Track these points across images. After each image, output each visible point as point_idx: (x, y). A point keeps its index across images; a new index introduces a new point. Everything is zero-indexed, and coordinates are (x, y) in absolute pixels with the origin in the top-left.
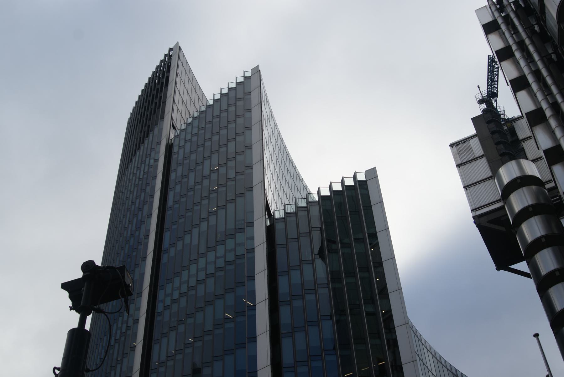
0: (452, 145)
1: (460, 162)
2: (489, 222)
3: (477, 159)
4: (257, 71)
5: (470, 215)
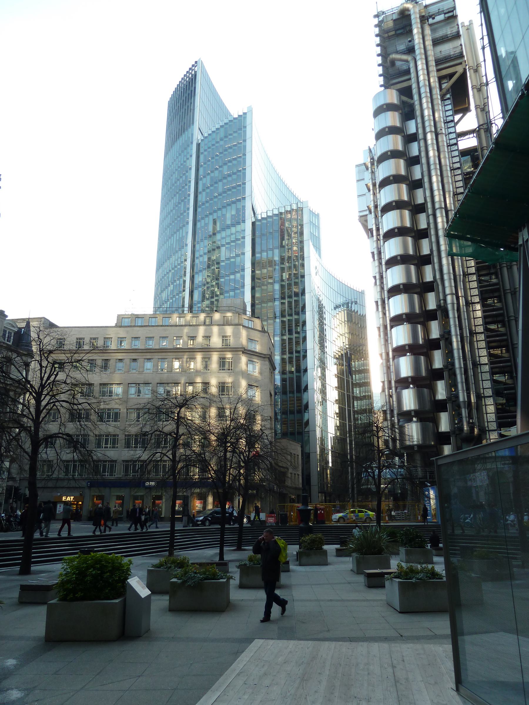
4: (250, 110)
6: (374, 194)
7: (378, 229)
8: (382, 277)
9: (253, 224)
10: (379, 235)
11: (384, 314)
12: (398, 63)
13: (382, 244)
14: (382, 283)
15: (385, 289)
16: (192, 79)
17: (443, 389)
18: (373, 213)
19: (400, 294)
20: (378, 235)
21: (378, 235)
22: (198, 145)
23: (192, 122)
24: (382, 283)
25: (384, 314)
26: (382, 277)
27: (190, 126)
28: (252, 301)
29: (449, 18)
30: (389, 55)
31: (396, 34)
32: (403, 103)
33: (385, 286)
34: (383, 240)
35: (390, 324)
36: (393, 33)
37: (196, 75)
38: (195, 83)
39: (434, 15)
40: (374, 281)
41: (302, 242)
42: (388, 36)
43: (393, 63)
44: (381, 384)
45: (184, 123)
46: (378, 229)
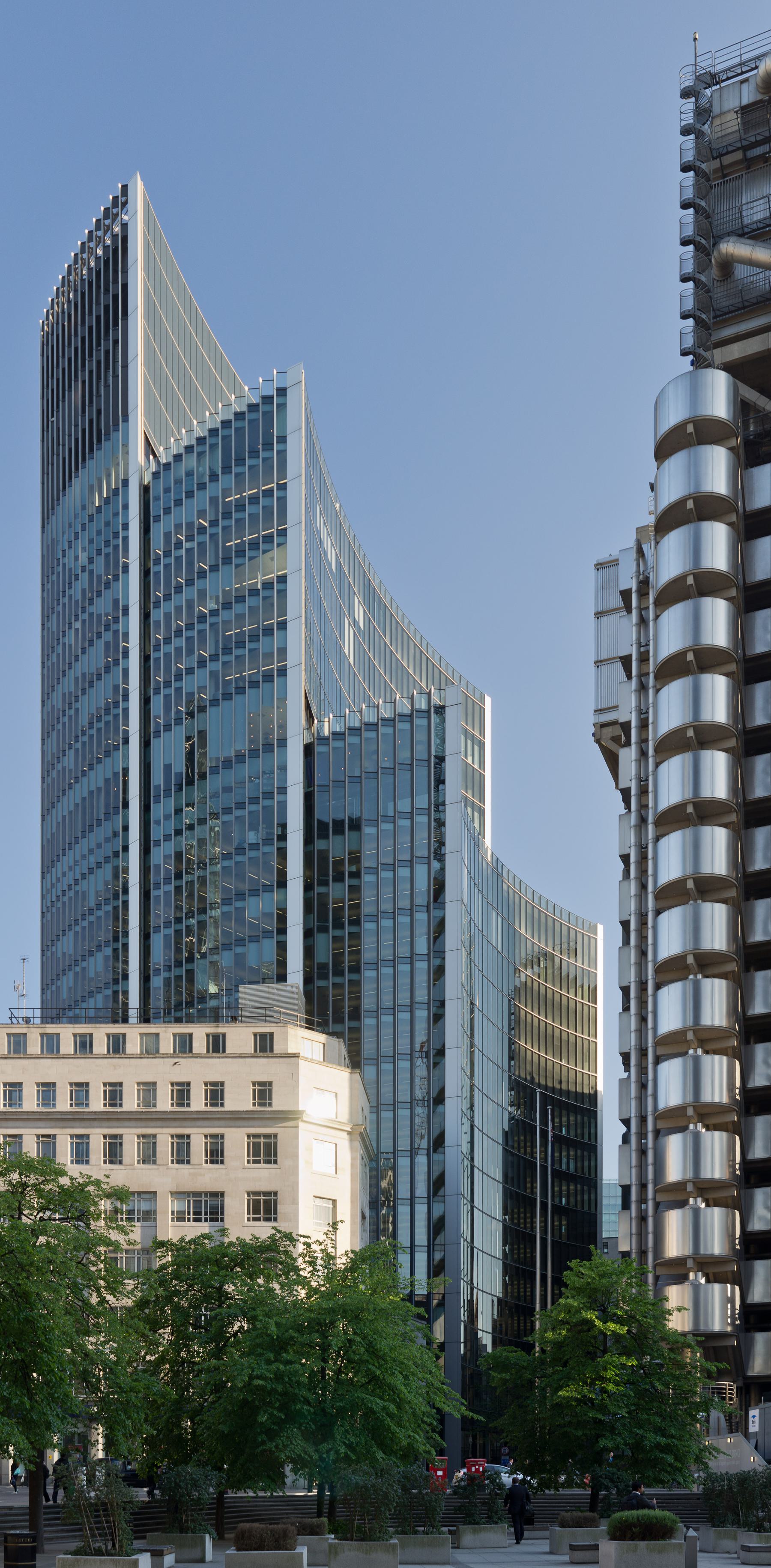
1: (600, 609)
6: (643, 621)
7: (644, 725)
8: (643, 857)
9: (308, 750)
10: (646, 741)
11: (643, 953)
12: (742, 272)
13: (651, 767)
14: (643, 871)
15: (650, 888)
16: (115, 251)
17: (766, 1208)
18: (634, 612)
19: (688, 827)
20: (643, 741)
21: (643, 741)
22: (145, 490)
24: (643, 871)
25: (643, 953)
26: (643, 857)
28: (305, 966)
30: (717, 240)
31: (745, 159)
33: (650, 880)
34: (655, 756)
35: (655, 979)
36: (739, 155)
38: (125, 271)
40: (622, 866)
41: (440, 806)
42: (722, 167)
43: (727, 266)
44: (597, 745)
45: (99, 412)
46: (644, 725)
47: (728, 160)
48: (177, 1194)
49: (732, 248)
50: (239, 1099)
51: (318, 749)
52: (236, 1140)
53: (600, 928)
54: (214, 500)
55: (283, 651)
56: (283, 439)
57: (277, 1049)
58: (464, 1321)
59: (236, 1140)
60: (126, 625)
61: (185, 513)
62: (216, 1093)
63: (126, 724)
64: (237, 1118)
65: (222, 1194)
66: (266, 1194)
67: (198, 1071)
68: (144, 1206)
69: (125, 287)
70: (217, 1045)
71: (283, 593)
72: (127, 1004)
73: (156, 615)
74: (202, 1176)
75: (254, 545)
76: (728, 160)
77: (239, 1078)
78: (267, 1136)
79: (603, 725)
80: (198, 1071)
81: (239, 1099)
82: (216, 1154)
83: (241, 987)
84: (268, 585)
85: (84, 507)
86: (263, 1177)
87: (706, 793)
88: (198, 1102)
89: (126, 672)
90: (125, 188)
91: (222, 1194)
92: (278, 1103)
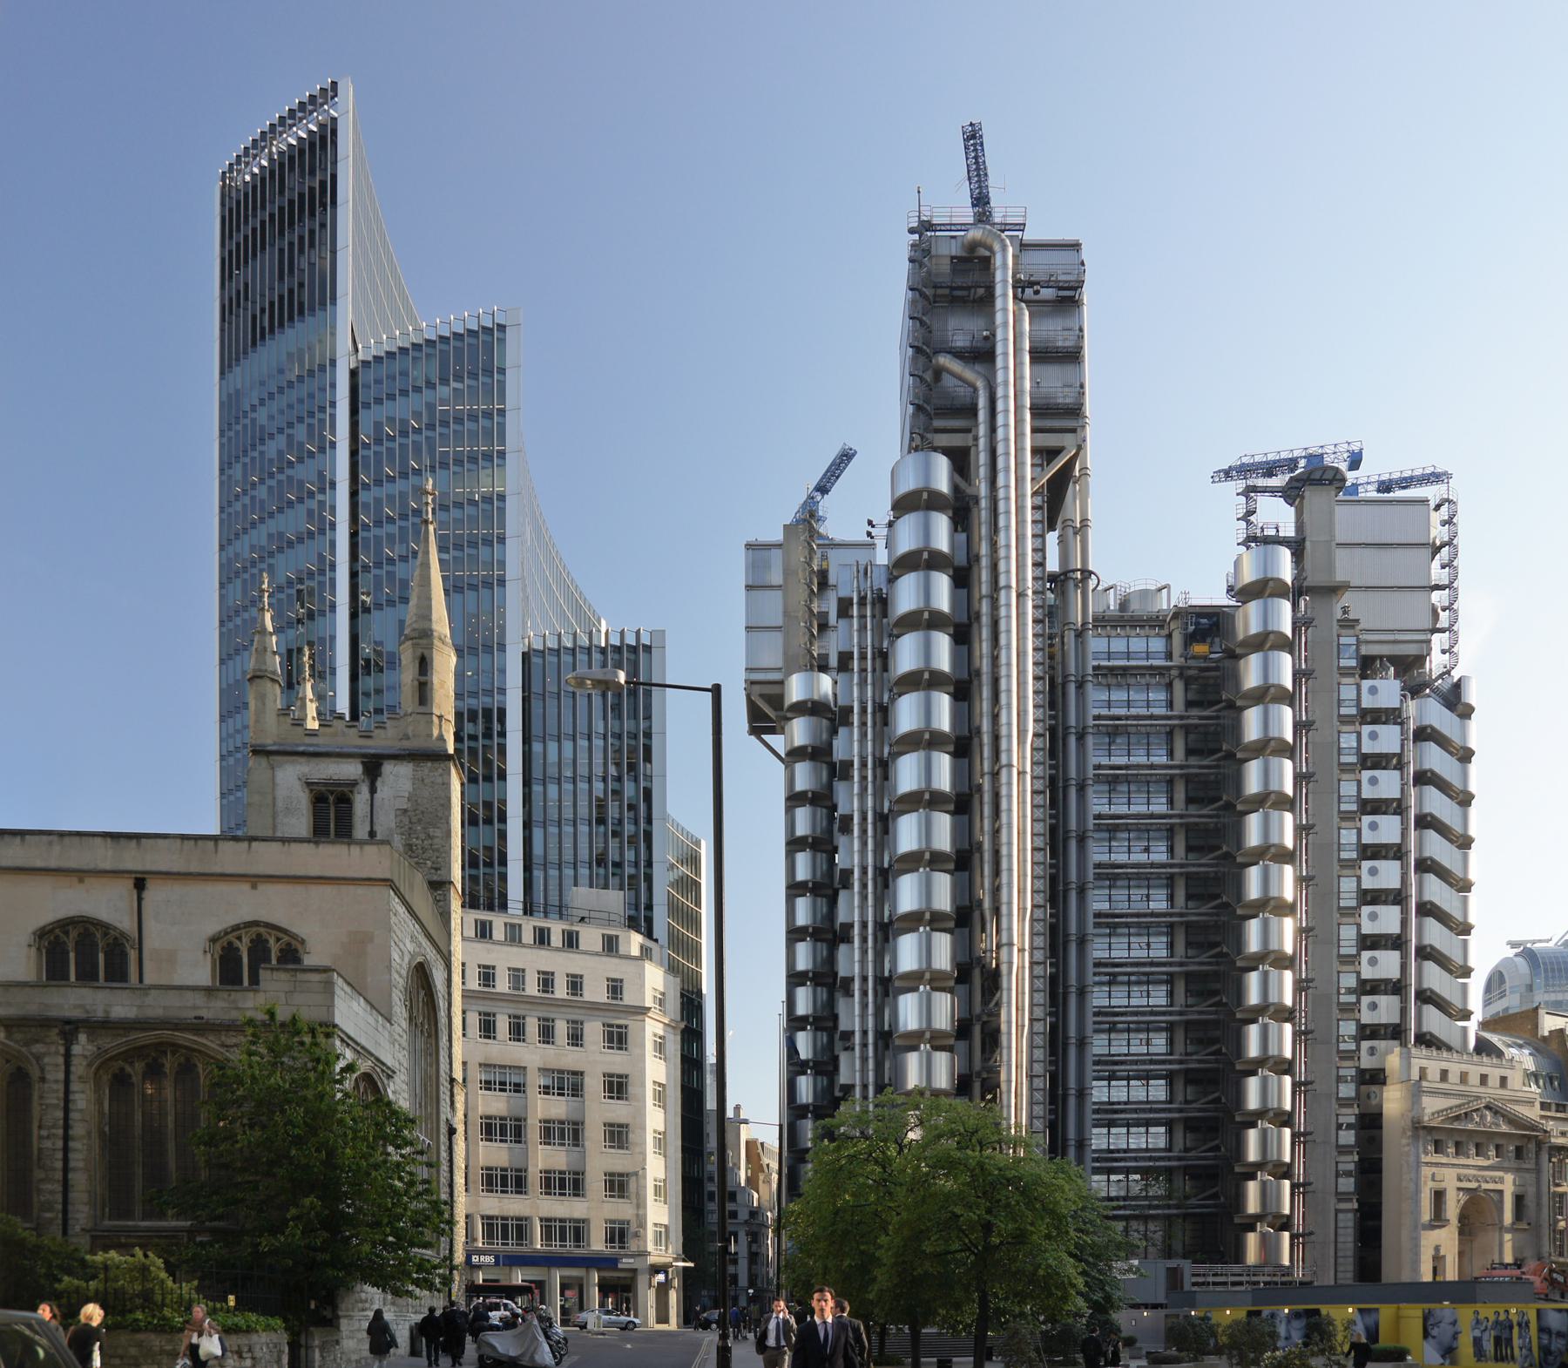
0: (749, 546)
2: (762, 696)
3: (771, 587)
5: (742, 676)
12: (948, 381)
23: (323, 294)
27: (323, 304)
29: (1064, 298)
32: (956, 488)
36: (947, 291)
37: (334, 132)
38: (335, 163)
39: (1038, 283)
47: (940, 291)
48: (544, 1071)
49: (943, 360)
50: (595, 992)
51: (536, 660)
52: (594, 1030)
53: (703, 843)
54: (431, 407)
55: (502, 564)
56: (502, 371)
57: (622, 950)
58: (1502, 1229)
59: (594, 1030)
60: (334, 498)
61: (400, 408)
62: (575, 984)
63: (333, 594)
64: (594, 1007)
65: (582, 1073)
66: (620, 1076)
67: (561, 964)
68: (515, 1079)
69: (334, 177)
70: (571, 941)
71: (502, 510)
72: (506, 896)
73: (363, 496)
74: (563, 1056)
75: (473, 459)
76: (940, 291)
77: (596, 974)
78: (619, 1026)
79: (753, 683)
80: (561, 964)
81: (595, 992)
82: (576, 1038)
83: (203, 815)
84: (487, 499)
85: (281, 371)
86: (616, 1062)
87: (935, 785)
88: (561, 991)
89: (333, 544)
90: (334, 84)
91: (582, 1073)
92: (628, 998)
